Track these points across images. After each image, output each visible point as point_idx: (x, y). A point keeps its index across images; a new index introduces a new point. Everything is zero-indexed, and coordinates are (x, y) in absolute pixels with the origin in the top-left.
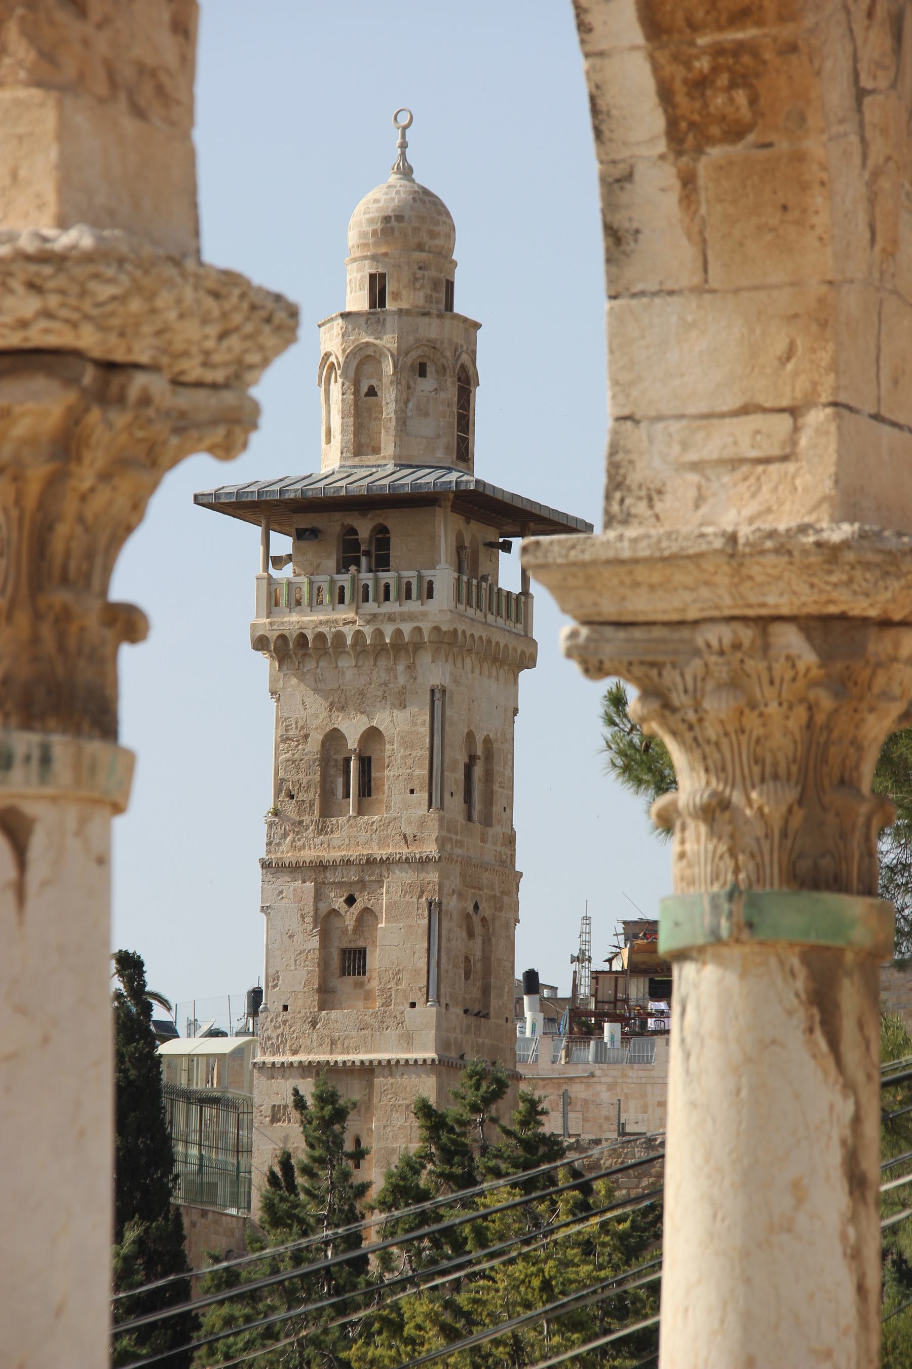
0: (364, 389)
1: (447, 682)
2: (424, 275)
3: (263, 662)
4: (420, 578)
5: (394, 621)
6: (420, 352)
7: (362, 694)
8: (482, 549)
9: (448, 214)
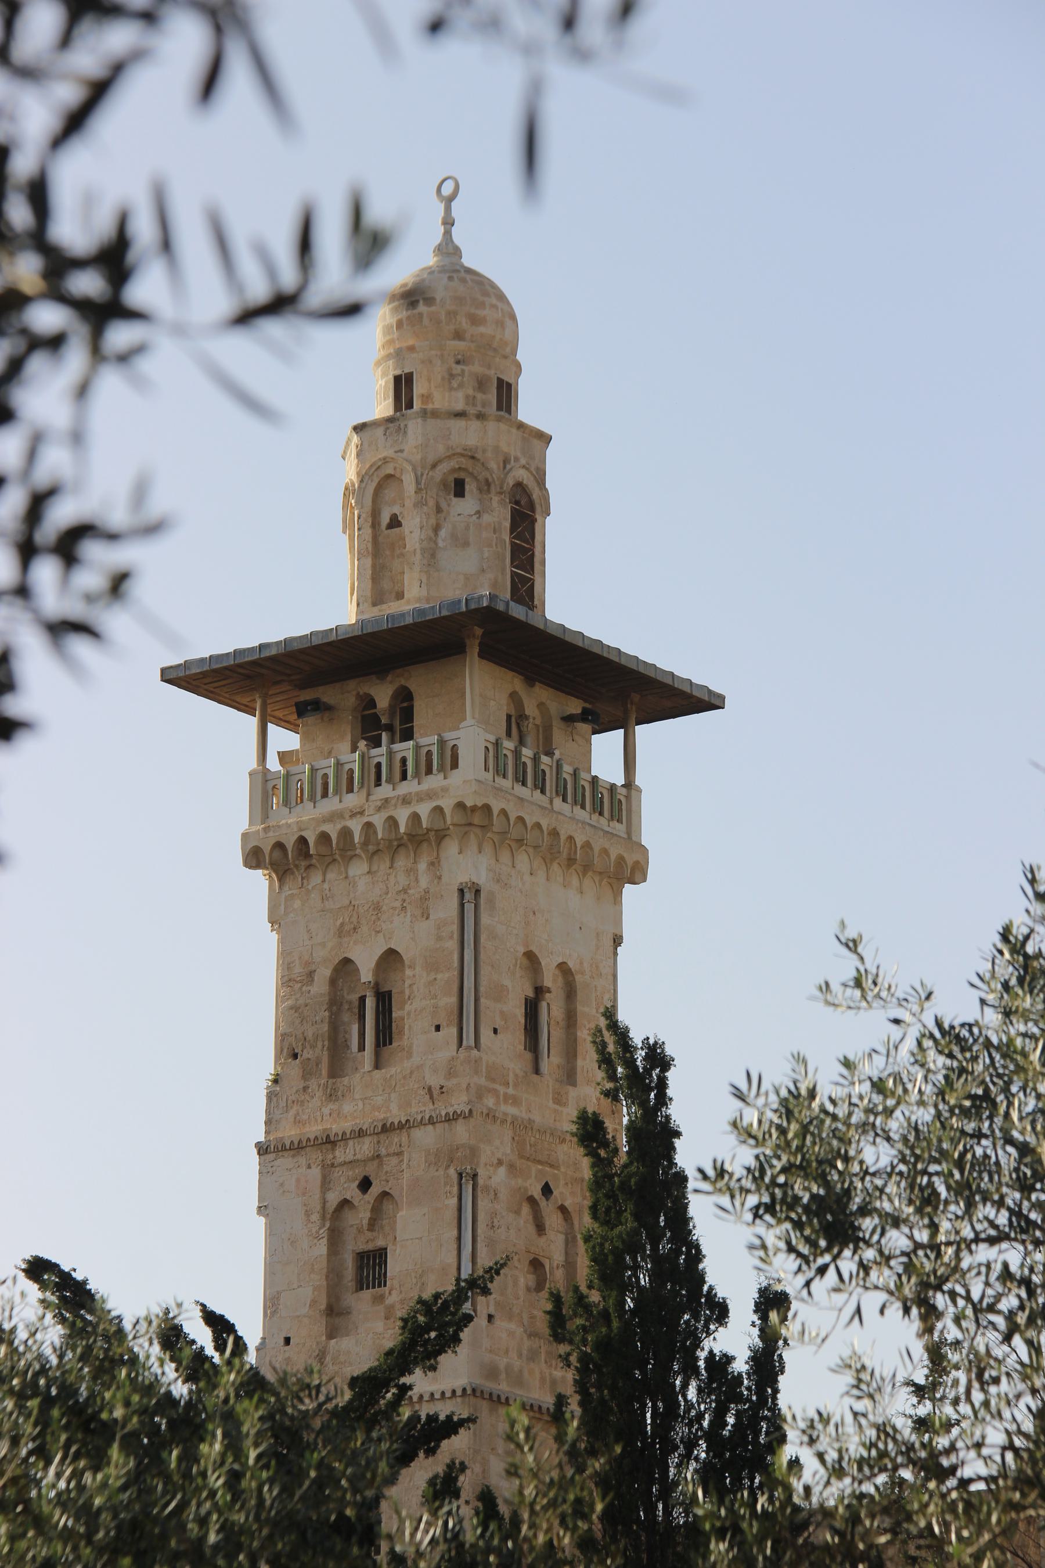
0: (385, 519)
1: (482, 879)
2: (463, 371)
3: (259, 881)
4: (442, 743)
5: (410, 803)
6: (453, 464)
7: (377, 908)
8: (557, 724)
9: (501, 297)
